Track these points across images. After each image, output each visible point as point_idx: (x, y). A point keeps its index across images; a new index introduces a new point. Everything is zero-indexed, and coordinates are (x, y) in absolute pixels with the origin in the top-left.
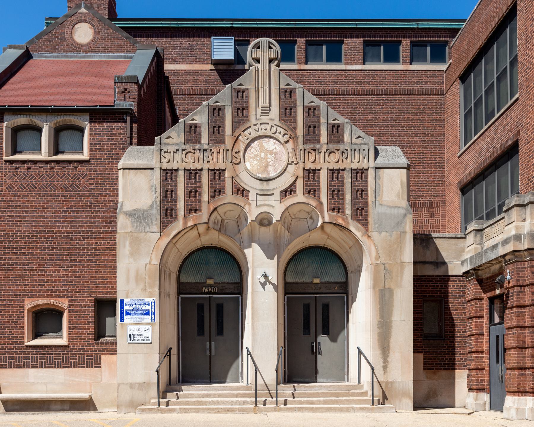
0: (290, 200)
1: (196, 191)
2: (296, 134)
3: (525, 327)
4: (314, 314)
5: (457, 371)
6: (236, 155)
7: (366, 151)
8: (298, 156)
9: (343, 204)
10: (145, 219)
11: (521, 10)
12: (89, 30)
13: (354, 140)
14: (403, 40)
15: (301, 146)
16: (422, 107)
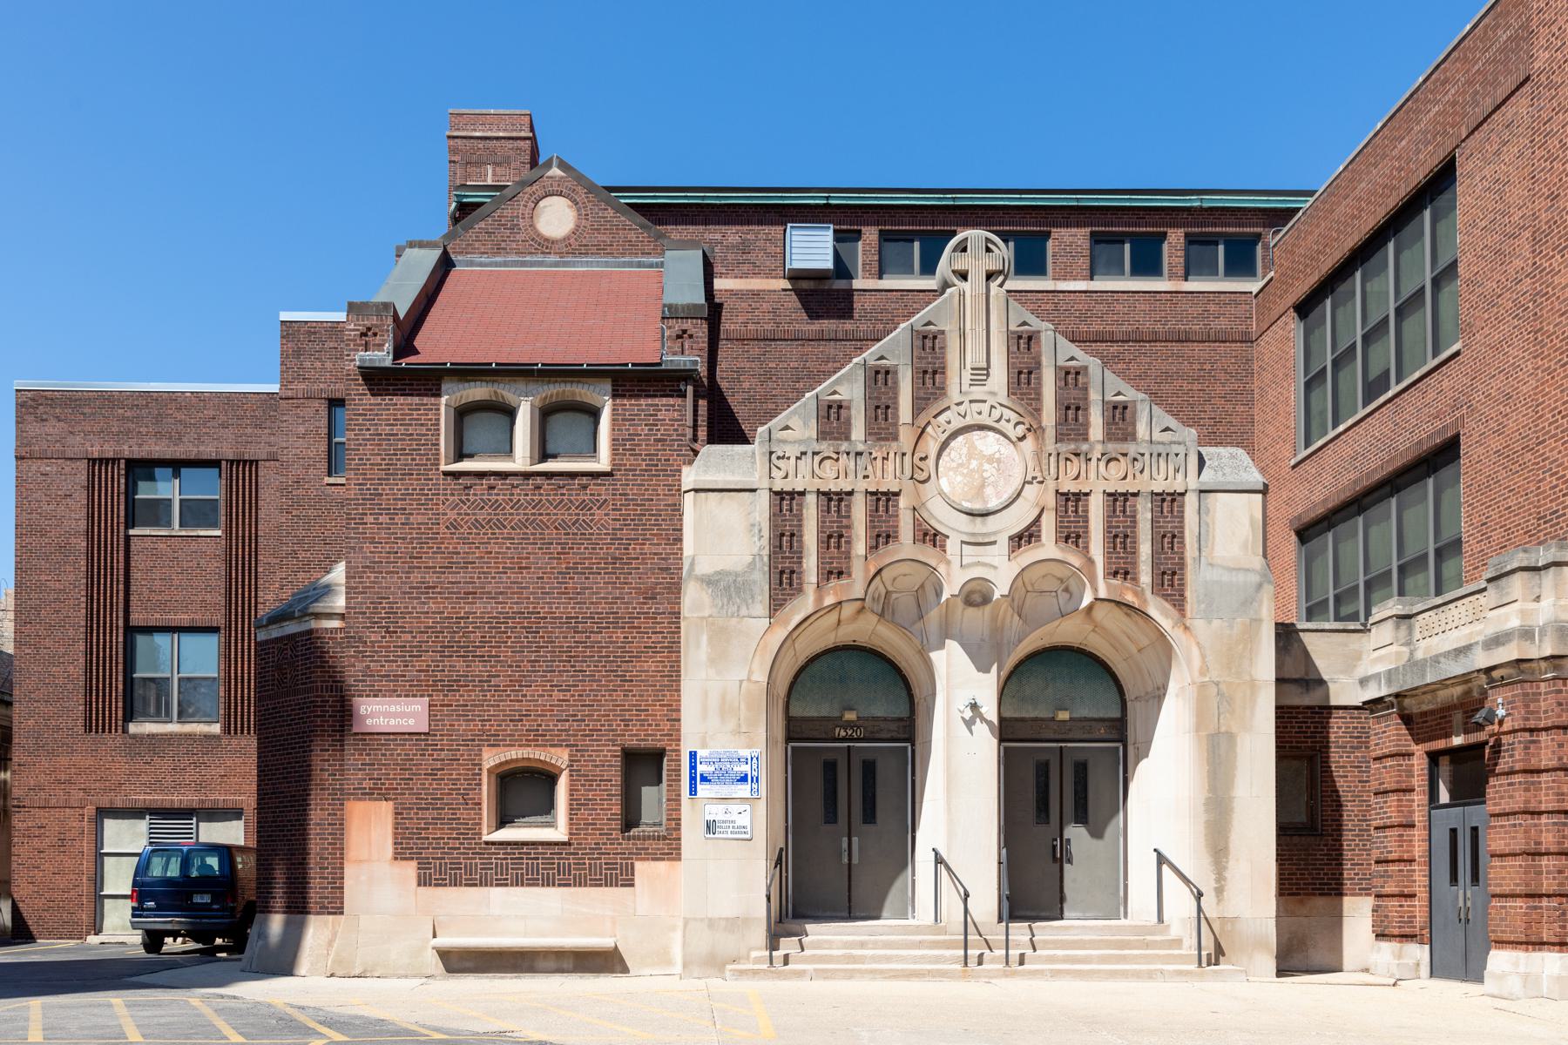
0: (1029, 555)
1: (841, 536)
2: (1040, 422)
3: (1540, 813)
4: (1062, 781)
5: (1346, 900)
6: (921, 464)
7: (1182, 456)
8: (1045, 467)
9: (1135, 564)
10: (738, 590)
11: (1470, 175)
12: (568, 210)
13: (1157, 436)
14: (1170, 231)
15: (1050, 446)
16: (1207, 367)
